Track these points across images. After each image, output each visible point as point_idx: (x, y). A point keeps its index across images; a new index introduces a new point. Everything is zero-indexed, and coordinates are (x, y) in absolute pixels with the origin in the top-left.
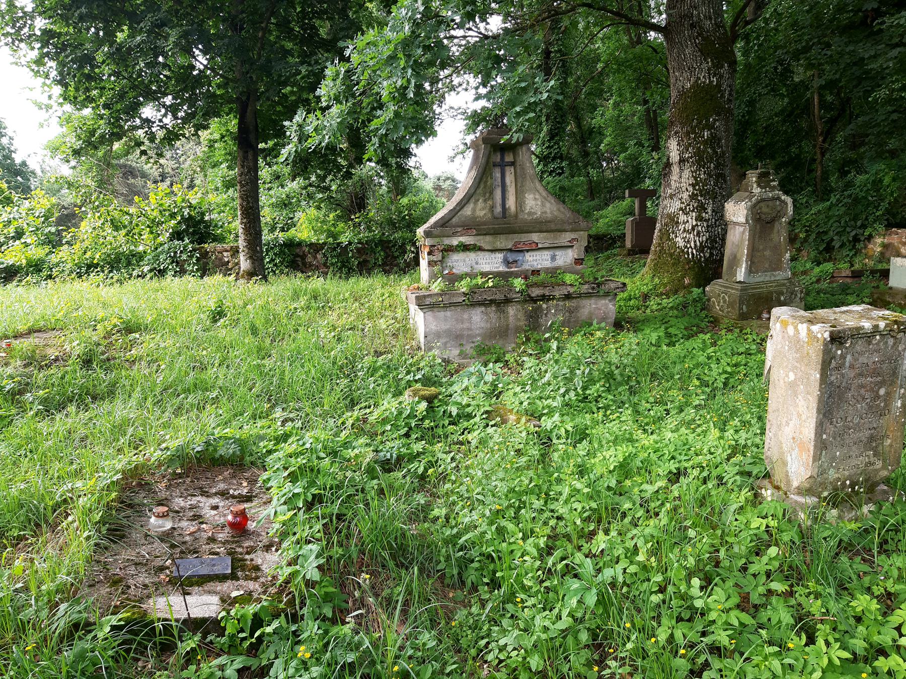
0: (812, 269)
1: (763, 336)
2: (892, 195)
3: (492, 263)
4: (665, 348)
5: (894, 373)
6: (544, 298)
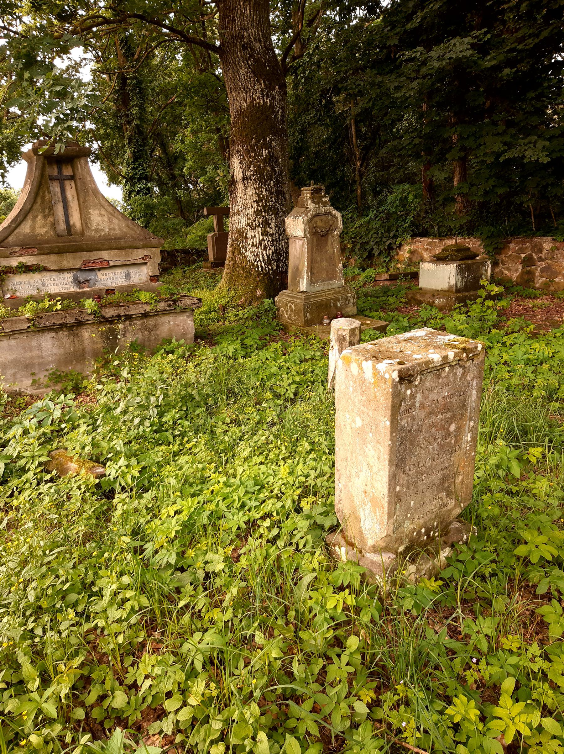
0: (359, 274)
1: (325, 340)
2: (415, 210)
3: (60, 284)
4: (241, 360)
5: (464, 405)
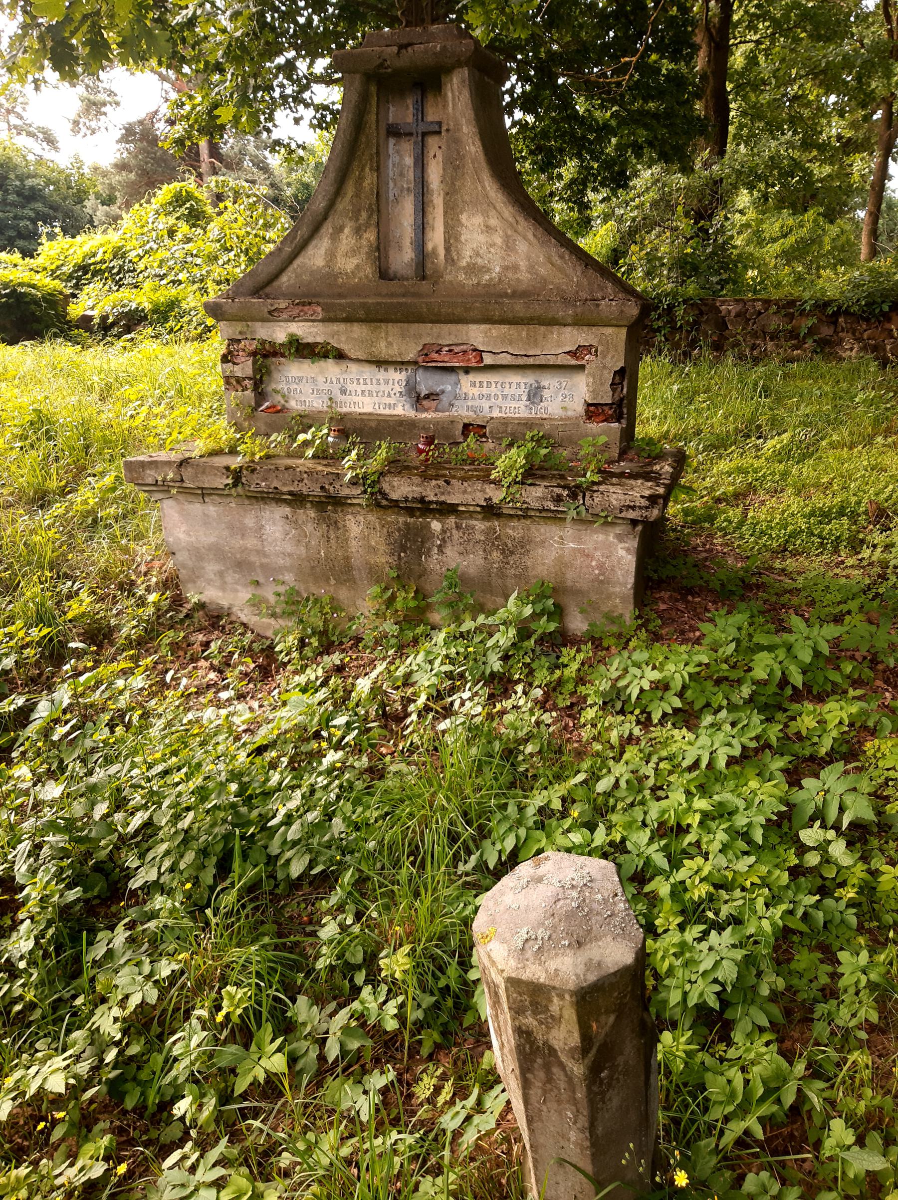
3: (375, 394)
6: (423, 508)
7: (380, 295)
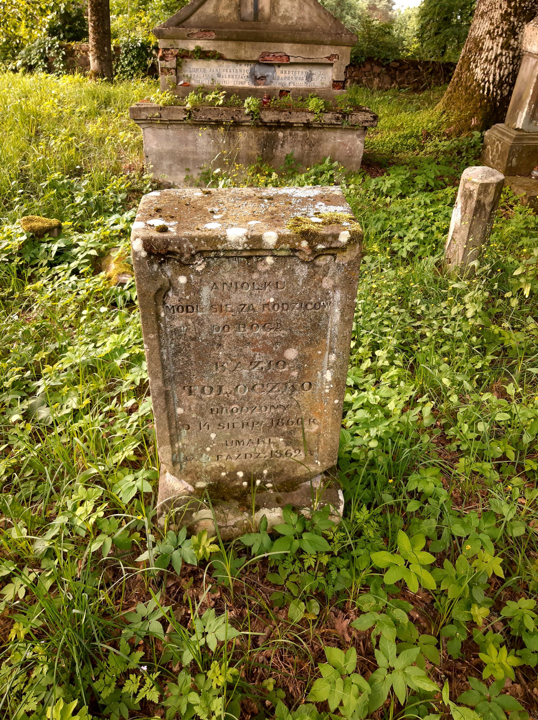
3: (235, 76)
5: (315, 327)
6: (279, 126)
7: (240, 28)
